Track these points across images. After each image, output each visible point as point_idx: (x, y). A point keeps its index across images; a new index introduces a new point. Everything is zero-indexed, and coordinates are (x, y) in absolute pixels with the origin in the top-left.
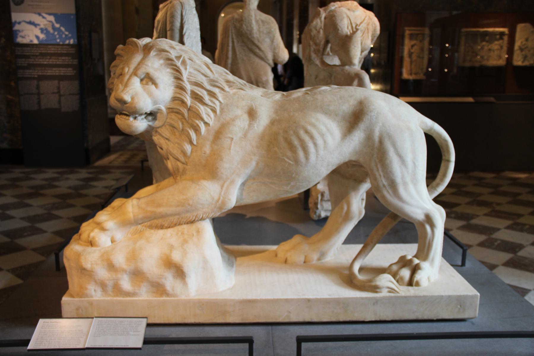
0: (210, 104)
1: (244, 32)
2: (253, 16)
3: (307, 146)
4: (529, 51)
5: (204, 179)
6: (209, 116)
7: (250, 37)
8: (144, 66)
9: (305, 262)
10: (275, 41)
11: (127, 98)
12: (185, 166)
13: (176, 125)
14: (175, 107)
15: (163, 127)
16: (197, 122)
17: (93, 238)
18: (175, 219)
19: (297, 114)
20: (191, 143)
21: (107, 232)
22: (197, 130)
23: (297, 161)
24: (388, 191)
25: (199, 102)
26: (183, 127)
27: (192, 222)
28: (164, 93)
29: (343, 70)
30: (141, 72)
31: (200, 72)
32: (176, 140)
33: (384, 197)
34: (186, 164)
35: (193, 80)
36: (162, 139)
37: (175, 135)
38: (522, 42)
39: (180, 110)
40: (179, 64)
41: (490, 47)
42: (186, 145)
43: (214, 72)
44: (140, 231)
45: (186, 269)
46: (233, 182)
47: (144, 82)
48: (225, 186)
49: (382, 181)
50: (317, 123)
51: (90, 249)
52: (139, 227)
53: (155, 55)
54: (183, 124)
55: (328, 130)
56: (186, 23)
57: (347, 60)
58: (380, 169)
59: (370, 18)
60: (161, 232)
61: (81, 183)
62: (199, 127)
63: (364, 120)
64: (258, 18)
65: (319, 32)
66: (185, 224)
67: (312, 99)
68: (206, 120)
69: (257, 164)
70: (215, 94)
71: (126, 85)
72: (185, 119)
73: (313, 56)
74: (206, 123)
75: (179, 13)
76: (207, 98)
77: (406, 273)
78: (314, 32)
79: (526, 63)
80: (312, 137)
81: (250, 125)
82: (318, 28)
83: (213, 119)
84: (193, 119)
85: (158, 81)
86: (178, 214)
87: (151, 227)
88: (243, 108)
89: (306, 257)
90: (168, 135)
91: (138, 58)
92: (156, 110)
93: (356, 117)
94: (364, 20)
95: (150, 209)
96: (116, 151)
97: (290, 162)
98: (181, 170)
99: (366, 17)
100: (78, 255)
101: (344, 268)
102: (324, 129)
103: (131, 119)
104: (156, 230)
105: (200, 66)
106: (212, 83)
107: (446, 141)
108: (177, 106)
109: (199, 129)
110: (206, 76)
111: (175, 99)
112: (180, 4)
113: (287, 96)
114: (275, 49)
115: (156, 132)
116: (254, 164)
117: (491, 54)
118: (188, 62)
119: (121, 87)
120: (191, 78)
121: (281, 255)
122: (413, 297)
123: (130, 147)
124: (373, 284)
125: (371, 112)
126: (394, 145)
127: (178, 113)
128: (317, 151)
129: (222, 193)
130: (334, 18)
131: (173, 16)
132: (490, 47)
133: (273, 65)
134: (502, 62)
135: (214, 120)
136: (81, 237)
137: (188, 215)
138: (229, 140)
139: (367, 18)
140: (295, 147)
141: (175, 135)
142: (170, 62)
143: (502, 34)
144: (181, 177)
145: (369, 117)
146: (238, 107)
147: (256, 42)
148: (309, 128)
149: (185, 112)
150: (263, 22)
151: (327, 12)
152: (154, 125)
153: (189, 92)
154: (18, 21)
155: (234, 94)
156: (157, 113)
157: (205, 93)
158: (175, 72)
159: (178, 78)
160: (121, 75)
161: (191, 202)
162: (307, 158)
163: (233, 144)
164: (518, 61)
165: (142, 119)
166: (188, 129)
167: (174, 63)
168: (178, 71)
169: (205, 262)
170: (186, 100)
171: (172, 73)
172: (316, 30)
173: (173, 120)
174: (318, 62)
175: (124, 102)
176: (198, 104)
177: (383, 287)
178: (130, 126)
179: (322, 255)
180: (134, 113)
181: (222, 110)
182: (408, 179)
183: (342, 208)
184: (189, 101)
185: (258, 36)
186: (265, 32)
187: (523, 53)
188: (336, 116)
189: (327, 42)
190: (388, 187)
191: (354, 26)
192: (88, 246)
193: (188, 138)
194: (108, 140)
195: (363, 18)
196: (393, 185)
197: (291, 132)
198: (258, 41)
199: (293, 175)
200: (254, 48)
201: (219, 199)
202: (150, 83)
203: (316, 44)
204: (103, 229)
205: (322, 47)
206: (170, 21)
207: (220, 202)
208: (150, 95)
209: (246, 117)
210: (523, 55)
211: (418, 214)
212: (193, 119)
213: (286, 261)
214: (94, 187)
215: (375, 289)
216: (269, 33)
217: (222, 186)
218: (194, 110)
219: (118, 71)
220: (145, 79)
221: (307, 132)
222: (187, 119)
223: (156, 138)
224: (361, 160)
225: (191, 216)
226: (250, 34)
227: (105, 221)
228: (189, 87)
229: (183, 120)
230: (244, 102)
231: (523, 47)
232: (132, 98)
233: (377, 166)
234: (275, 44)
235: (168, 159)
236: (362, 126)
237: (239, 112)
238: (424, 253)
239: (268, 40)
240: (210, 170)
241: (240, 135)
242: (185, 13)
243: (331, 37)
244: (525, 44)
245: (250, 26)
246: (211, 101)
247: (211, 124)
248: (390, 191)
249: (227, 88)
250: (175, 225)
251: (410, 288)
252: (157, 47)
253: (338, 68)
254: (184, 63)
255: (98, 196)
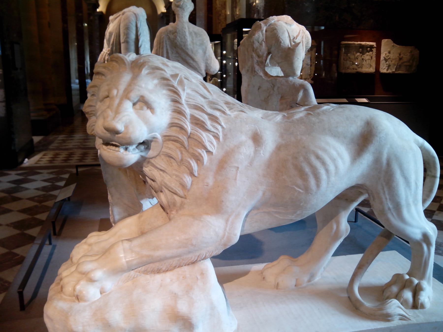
0: (213, 130)
1: (178, 43)
2: (187, 28)
3: (319, 173)
4: (392, 61)
5: (207, 214)
6: (212, 143)
7: (184, 48)
8: (137, 87)
9: (295, 286)
10: (207, 52)
11: (120, 127)
12: (183, 199)
13: (173, 154)
14: (173, 134)
15: (158, 157)
16: (199, 151)
17: (81, 292)
18: (175, 262)
19: (304, 138)
20: (192, 174)
21: (96, 283)
22: (198, 159)
23: (307, 189)
24: (392, 214)
25: (200, 129)
26: (182, 157)
27: (193, 263)
28: (161, 117)
29: (287, 81)
30: (134, 96)
31: (198, 93)
32: (174, 172)
33: (388, 220)
34: (185, 198)
35: (192, 102)
36: (156, 170)
37: (172, 166)
38: (386, 54)
39: (179, 138)
40: (175, 84)
41: (363, 57)
42: (186, 177)
43: (212, 93)
44: (134, 278)
45: (194, 321)
46: (238, 215)
47: (138, 106)
48: (231, 219)
49: (387, 204)
50: (327, 147)
51: (78, 306)
52: (132, 273)
53: (148, 74)
54: (182, 153)
55: (338, 154)
56: (142, 35)
57: (289, 70)
58: (387, 192)
59: (304, 32)
60: (158, 277)
61: (13, 185)
62: (202, 157)
63: (374, 142)
64: (191, 30)
65: (261, 44)
66: (185, 265)
67: (317, 120)
68: (209, 149)
69: (264, 194)
70: (217, 118)
71: (117, 112)
72: (185, 148)
73: (257, 68)
74: (208, 152)
75: (134, 24)
76: (209, 124)
77: (408, 295)
78: (256, 45)
79: (390, 71)
80: (324, 163)
81: (256, 151)
82: (260, 41)
83: (216, 147)
84: (194, 148)
85: (155, 105)
86: (179, 256)
87: (146, 272)
88: (247, 135)
89: (297, 280)
90: (163, 166)
91: (126, 78)
92: (150, 139)
93: (365, 139)
94: (299, 33)
95: (146, 252)
96: (39, 151)
97: (300, 190)
98: (178, 205)
99: (300, 31)
100: (66, 315)
101: (342, 290)
102: (334, 154)
103: (122, 150)
104: (153, 275)
105: (198, 86)
106: (212, 105)
107: (434, 157)
108: (174, 132)
109: (201, 158)
110: (205, 98)
111: (172, 125)
112: (134, 15)
113: (288, 118)
114: (207, 60)
115: (149, 162)
116: (260, 193)
117: (364, 63)
118: (185, 81)
119: (110, 113)
120: (190, 100)
121: (271, 279)
122: (426, 323)
123: (51, 147)
124: (384, 312)
125: (379, 133)
126: (401, 167)
127: (177, 141)
128: (328, 177)
129: (228, 229)
130: (275, 31)
131: (127, 28)
132: (363, 57)
133: (205, 76)
134: (372, 70)
135: (217, 147)
136: (64, 290)
137: (190, 256)
138: (234, 170)
139: (301, 32)
140: (307, 174)
141: (172, 166)
142: (166, 82)
143: (371, 47)
144: (177, 211)
145: (378, 139)
146: (241, 132)
147: (190, 53)
148: (320, 153)
149: (184, 139)
150: (196, 33)
151: (267, 25)
152: (147, 156)
153: (189, 117)
154: (295, 36)
155: (236, 117)
156: (151, 141)
157: (206, 117)
158: (172, 94)
159: (176, 101)
160: (108, 97)
161: (194, 242)
162: (318, 185)
163: (238, 174)
164: (383, 69)
165: (134, 149)
166: (189, 160)
167: (171, 83)
168: (176, 92)
169: (213, 308)
170: (186, 126)
171: (169, 96)
172: (258, 42)
173: (170, 149)
174: (261, 74)
175: (116, 132)
176: (200, 131)
177: (395, 315)
178: (120, 159)
179: (312, 276)
180: (126, 144)
181: (225, 135)
182: (411, 200)
183: (332, 228)
184: (189, 127)
185: (192, 47)
186: (198, 43)
187: (387, 63)
188: (345, 138)
189: (269, 53)
190: (392, 210)
191: (292, 39)
192: (74, 302)
193: (189, 170)
194: (32, 140)
195: (298, 31)
196: (398, 208)
197: (301, 159)
198: (192, 51)
199: (301, 205)
200: (188, 58)
201: (224, 235)
202: (145, 108)
203: (259, 56)
204: (91, 281)
205: (264, 58)
206: (124, 33)
207: (225, 238)
208: (146, 122)
209: (250, 143)
210: (387, 64)
211: (416, 233)
212: (194, 148)
213: (277, 286)
214: (27, 189)
215: (387, 317)
216: (202, 44)
217: (227, 221)
218: (195, 137)
219: (103, 93)
220: (139, 103)
221: (318, 157)
222: (187, 148)
223: (147, 170)
224: (368, 183)
225: (192, 257)
226: (185, 46)
227: (93, 270)
228: (188, 111)
229: (183, 149)
230: (247, 126)
231: (387, 58)
232: (126, 127)
233: (383, 189)
234: (207, 55)
235: (161, 192)
236: (372, 148)
237: (243, 138)
238: (418, 269)
239: (200, 52)
240: (214, 203)
241: (246, 163)
242: (141, 25)
243: (273, 49)
244: (388, 56)
245: (184, 37)
246: (214, 127)
247: (214, 151)
248: (394, 214)
249: (228, 112)
250: (175, 267)
251: (416, 311)
252: (150, 64)
253: (281, 79)
254: (181, 83)
255: (31, 199)
